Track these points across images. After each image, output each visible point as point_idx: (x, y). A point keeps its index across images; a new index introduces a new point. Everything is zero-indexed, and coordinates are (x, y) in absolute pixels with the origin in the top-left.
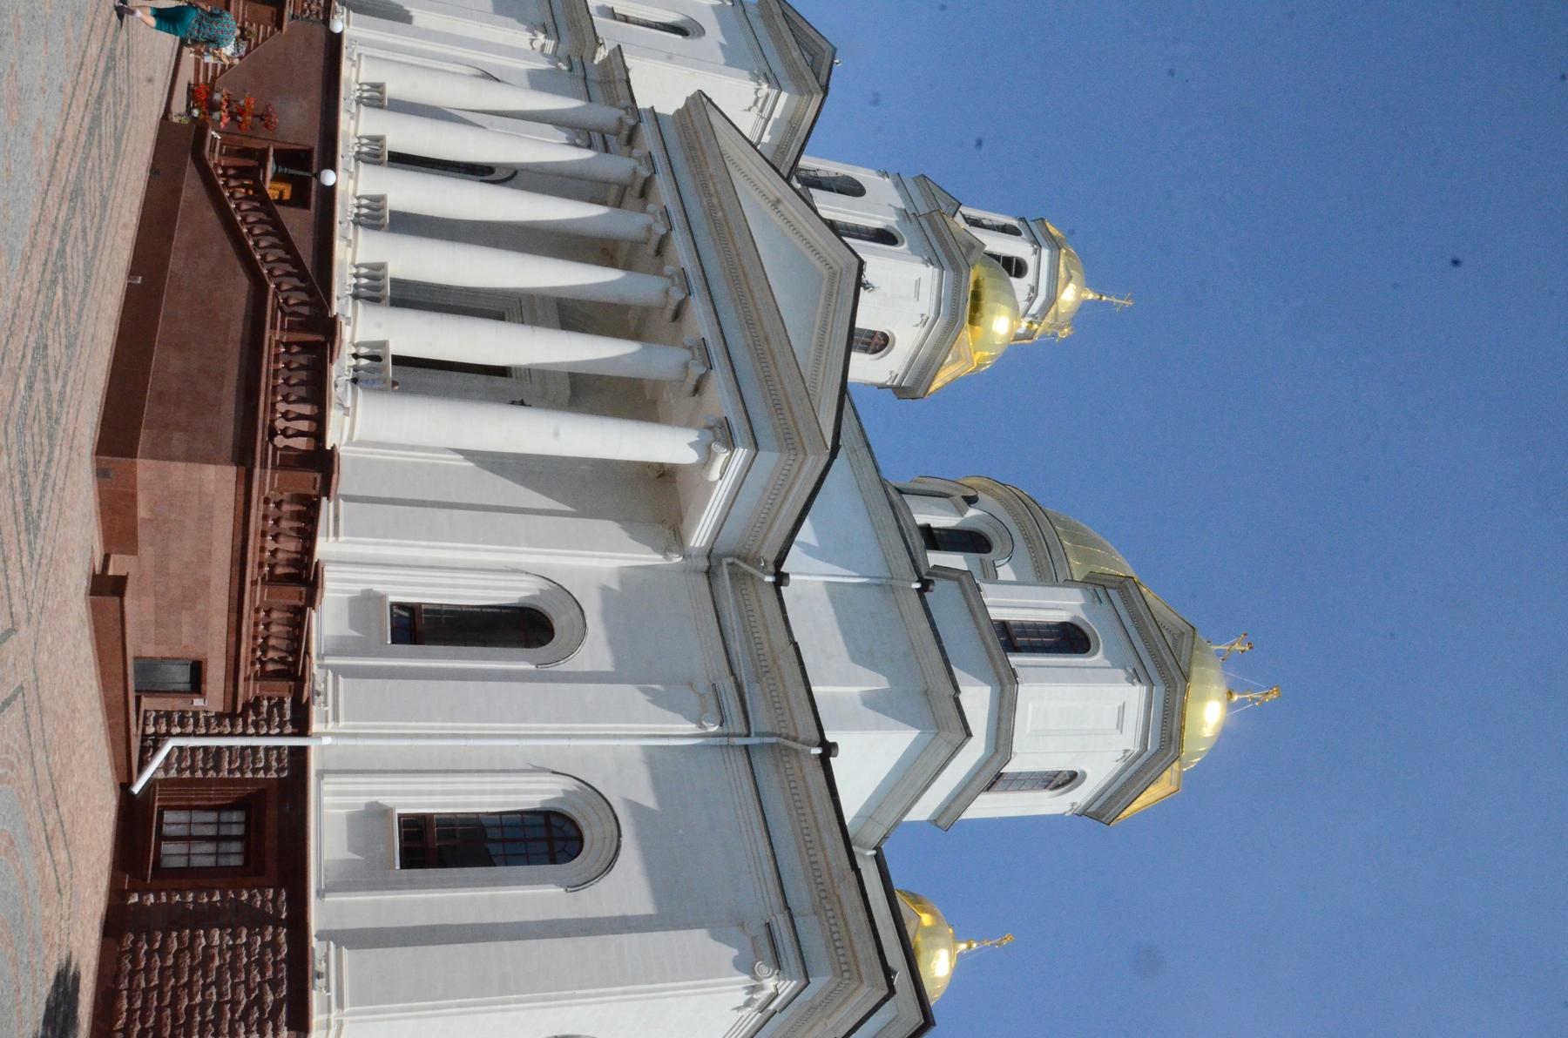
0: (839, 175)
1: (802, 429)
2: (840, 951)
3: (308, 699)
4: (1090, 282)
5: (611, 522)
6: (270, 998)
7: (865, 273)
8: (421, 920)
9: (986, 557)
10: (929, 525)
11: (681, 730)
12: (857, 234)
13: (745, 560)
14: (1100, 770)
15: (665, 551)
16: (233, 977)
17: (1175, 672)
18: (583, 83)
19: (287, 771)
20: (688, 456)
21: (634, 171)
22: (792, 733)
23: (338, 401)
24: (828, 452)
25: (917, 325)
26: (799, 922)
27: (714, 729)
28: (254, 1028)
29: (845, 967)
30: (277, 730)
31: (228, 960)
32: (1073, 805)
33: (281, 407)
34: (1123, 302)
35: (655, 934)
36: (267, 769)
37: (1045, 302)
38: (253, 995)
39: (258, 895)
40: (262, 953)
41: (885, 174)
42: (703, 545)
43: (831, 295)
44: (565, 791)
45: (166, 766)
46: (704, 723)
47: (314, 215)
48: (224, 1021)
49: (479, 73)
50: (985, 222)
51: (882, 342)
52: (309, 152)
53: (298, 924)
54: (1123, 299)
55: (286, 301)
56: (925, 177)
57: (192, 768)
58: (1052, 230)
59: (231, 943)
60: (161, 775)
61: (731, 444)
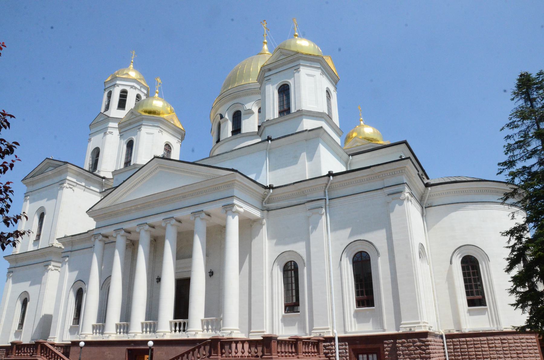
0: (91, 156)
1: (227, 181)
2: (396, 173)
3: (323, 338)
4: (127, 66)
5: (252, 243)
6: (418, 343)
7: (158, 156)
8: (391, 300)
10: (232, 131)
11: (324, 221)
13: (264, 199)
14: (326, 83)
15: (262, 225)
16: (413, 354)
17: (296, 56)
18: (72, 252)
19: (346, 343)
20: (237, 218)
21: (122, 236)
22: (325, 185)
23: (229, 335)
24: (235, 173)
25: (162, 134)
27: (324, 210)
28: (427, 347)
29: (401, 172)
30: (333, 346)
31: (407, 356)
32: (334, 91)
33: (234, 354)
34: (134, 54)
35: (393, 229)
36: (345, 349)
37: (136, 83)
38: (418, 348)
39: (386, 349)
40: (405, 347)
41: (90, 140)
42: (260, 212)
43: (171, 168)
44: (346, 257)
46: (322, 213)
47: (155, 347)
48: (426, 356)
50: (106, 104)
51: (168, 146)
52: (129, 350)
53: (394, 337)
54: (133, 54)
55: (204, 355)
56: (90, 125)
58: (109, 79)
59: (402, 356)
61: (233, 205)
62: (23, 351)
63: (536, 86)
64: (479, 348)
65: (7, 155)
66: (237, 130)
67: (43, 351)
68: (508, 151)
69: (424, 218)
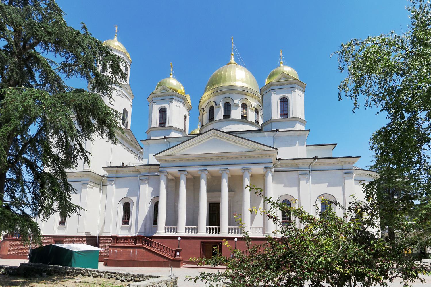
4: (113, 38)
12: (232, 205)
14: (185, 112)
26: (83, 180)
49: (86, 164)
62: (276, 280)
63: (79, 272)
65: (29, 126)
66: (227, 116)
68: (369, 196)
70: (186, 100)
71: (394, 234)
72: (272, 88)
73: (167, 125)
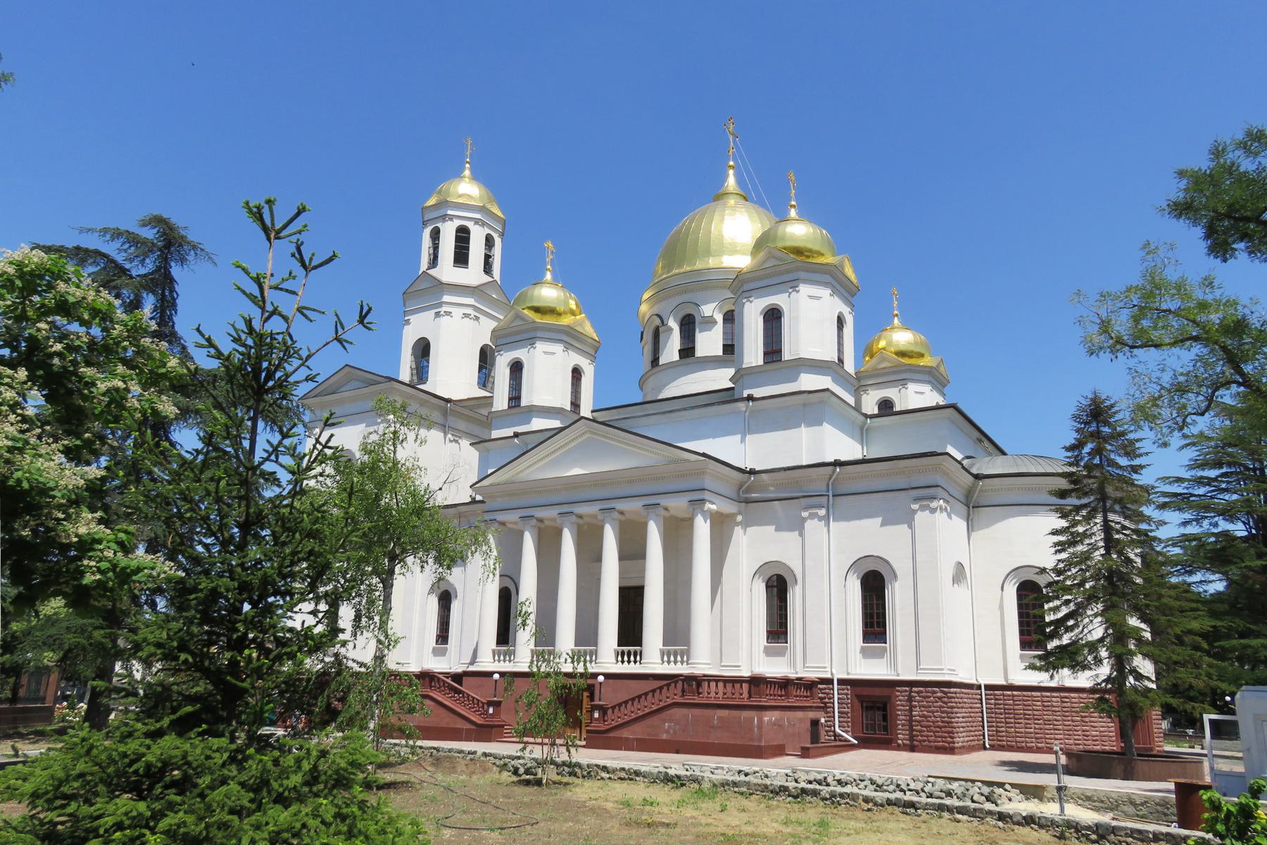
4: (458, 175)
6: (939, 694)
9: (697, 320)
22: (828, 476)
36: (847, 694)
40: (922, 697)
45: (846, 732)
54: (467, 145)
57: (847, 722)
60: (850, 733)
64: (1030, 706)
66: (687, 351)
67: (433, 684)
69: (970, 523)
70: (583, 337)
71: (27, 311)
72: (746, 287)
73: (787, 355)
